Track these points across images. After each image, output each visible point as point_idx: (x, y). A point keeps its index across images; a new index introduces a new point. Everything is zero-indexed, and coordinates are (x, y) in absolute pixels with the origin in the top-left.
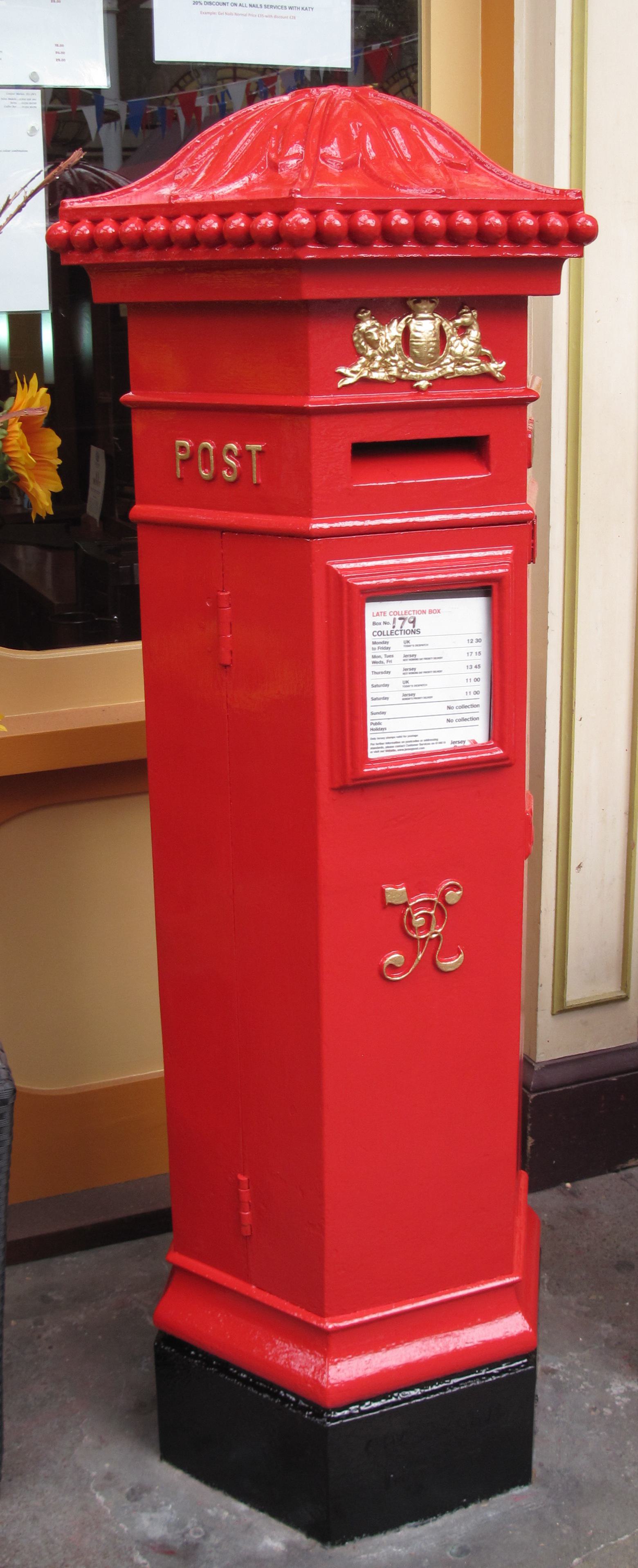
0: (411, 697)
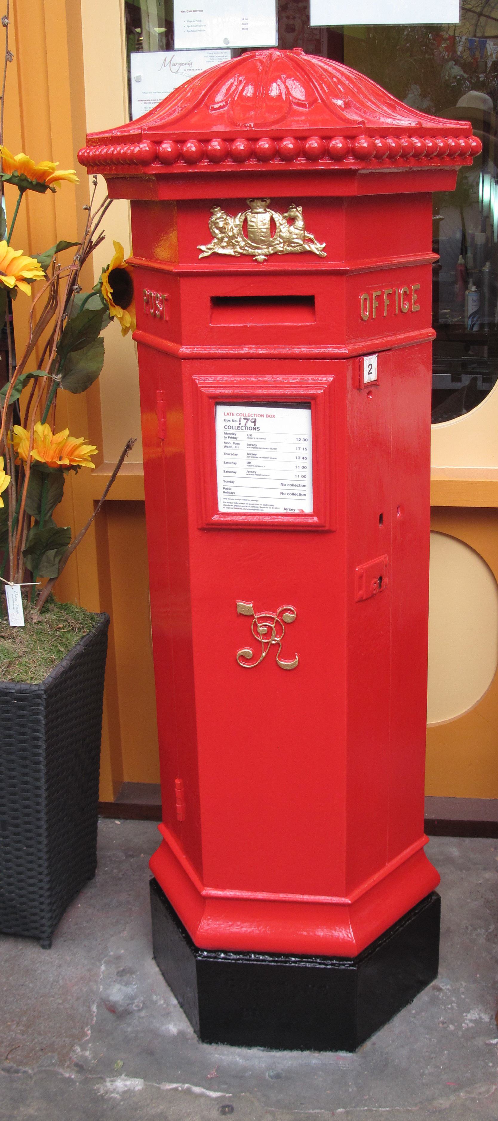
0: (253, 473)
